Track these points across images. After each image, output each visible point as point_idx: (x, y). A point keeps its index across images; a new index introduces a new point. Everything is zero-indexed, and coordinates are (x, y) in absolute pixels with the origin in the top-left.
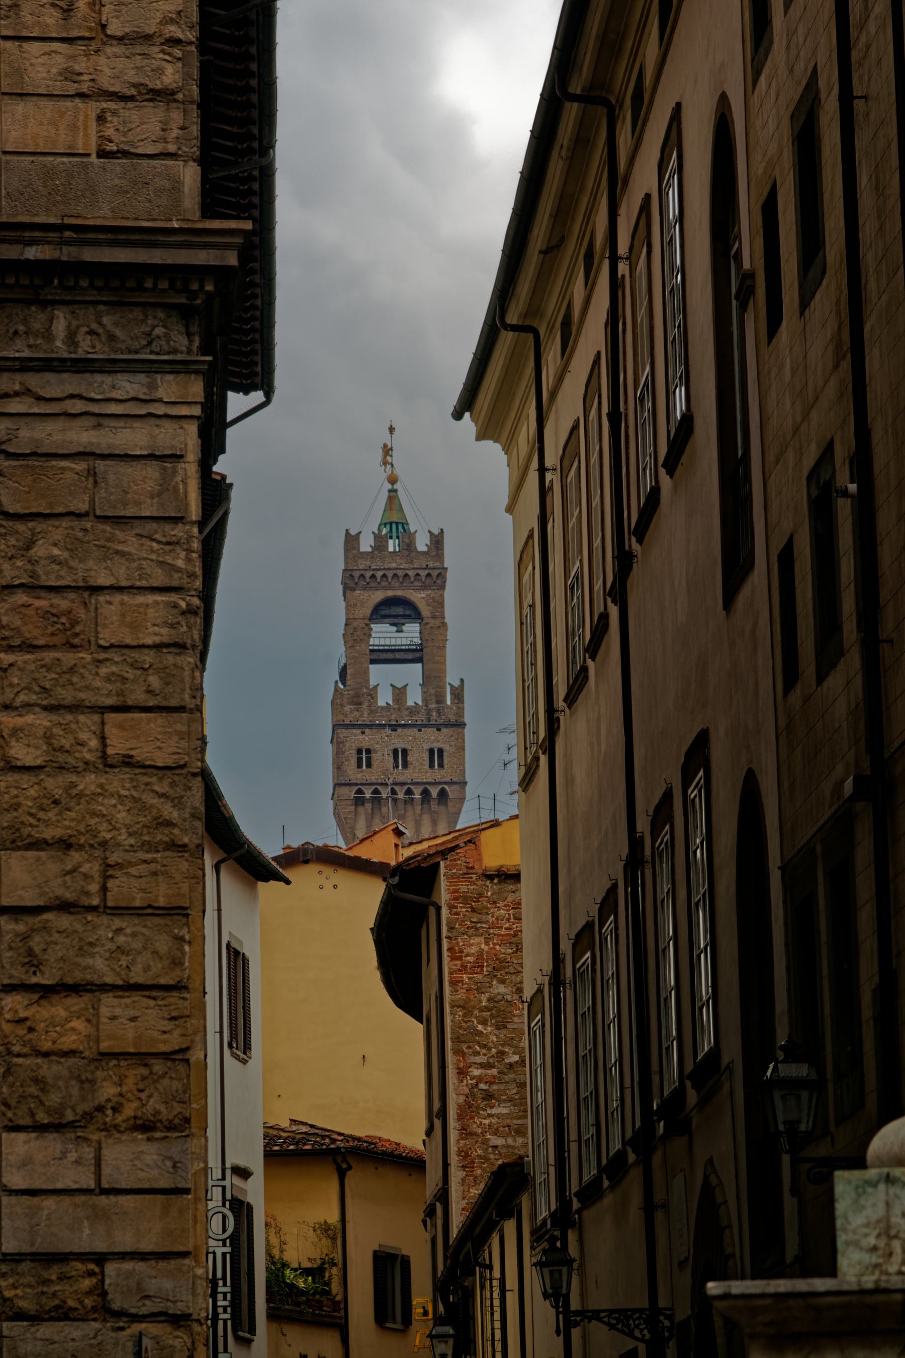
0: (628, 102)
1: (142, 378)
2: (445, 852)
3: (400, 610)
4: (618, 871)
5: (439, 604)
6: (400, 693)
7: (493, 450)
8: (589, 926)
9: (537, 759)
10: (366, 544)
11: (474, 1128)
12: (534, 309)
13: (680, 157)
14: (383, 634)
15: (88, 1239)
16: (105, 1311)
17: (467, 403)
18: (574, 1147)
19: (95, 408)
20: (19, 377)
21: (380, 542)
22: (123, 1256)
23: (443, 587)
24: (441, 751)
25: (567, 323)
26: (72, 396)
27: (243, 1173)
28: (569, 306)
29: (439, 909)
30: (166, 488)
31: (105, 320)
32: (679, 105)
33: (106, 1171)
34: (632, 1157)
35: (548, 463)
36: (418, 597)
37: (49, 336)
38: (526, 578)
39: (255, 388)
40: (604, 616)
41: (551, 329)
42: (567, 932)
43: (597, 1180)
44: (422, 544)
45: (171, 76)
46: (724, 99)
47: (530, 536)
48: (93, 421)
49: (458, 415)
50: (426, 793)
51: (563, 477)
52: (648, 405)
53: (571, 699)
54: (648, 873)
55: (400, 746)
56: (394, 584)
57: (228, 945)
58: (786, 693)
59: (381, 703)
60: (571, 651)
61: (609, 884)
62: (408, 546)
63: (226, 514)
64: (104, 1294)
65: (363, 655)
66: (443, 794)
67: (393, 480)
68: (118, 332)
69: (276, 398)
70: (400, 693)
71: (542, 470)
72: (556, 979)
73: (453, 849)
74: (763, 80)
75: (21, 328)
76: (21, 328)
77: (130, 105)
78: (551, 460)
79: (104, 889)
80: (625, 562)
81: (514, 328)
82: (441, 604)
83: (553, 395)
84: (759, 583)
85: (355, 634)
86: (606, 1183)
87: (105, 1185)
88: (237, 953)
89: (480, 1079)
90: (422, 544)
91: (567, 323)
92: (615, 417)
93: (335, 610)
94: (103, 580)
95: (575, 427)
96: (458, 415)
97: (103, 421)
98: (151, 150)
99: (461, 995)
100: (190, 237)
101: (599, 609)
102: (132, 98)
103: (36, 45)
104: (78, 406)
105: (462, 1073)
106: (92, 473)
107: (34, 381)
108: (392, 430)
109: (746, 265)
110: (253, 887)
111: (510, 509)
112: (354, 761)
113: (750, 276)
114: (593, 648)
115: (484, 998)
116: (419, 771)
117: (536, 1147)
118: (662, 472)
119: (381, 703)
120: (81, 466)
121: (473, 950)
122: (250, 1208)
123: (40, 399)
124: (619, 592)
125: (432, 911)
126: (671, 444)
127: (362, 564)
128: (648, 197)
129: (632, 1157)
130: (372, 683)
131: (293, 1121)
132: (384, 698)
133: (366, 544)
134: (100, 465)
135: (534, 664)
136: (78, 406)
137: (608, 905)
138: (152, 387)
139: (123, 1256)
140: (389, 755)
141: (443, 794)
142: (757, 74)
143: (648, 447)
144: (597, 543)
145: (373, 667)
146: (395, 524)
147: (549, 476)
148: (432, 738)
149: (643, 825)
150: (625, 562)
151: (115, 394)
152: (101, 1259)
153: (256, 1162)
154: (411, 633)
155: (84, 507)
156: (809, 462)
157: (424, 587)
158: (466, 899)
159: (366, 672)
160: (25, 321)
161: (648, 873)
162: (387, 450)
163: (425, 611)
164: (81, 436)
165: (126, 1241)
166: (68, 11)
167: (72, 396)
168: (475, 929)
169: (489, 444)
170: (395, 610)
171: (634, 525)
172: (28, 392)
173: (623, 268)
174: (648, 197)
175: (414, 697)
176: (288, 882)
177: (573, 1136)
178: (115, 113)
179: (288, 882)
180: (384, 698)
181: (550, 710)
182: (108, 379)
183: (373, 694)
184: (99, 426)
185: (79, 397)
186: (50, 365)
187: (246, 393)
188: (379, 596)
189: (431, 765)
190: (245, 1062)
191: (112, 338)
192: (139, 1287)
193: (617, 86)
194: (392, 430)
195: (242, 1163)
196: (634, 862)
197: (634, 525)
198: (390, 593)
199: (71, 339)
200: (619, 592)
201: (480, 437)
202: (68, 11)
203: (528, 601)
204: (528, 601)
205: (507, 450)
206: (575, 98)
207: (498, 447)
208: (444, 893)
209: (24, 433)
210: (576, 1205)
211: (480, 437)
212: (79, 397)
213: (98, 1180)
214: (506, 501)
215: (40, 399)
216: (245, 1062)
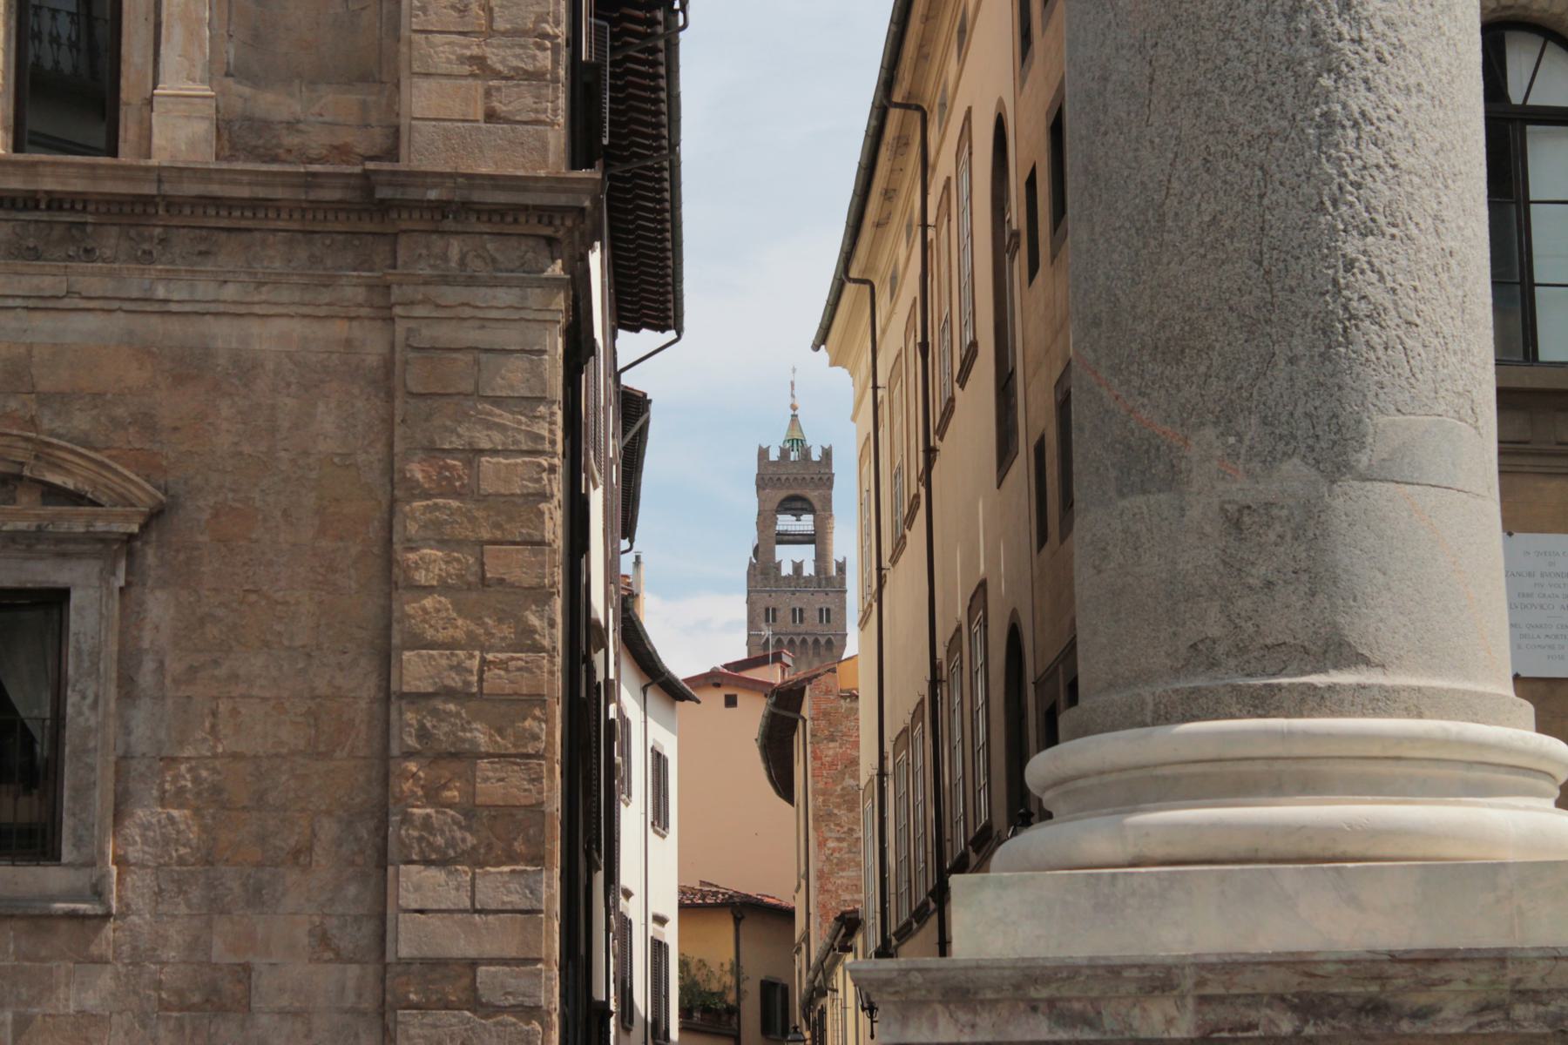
0: (936, 109)
1: (516, 291)
2: (809, 680)
3: (799, 505)
4: (925, 691)
5: (827, 501)
6: (798, 567)
7: (841, 373)
8: (905, 730)
9: (870, 605)
10: (774, 455)
11: (829, 886)
12: (870, 266)
13: (970, 147)
14: (786, 522)
15: (463, 947)
16: (475, 1003)
17: (822, 338)
18: (893, 897)
19: (480, 314)
20: (422, 289)
21: (784, 454)
22: (491, 961)
23: (831, 487)
24: (828, 610)
25: (894, 278)
26: (463, 304)
27: (661, 920)
28: (896, 266)
29: (805, 721)
30: (536, 373)
31: (489, 246)
32: (970, 109)
33: (479, 896)
34: (932, 906)
35: (879, 383)
36: (813, 495)
37: (445, 258)
38: (865, 470)
39: (669, 328)
40: (917, 496)
41: (883, 282)
42: (889, 736)
43: (909, 923)
44: (816, 455)
45: (545, 60)
46: (1001, 102)
47: (868, 438)
48: (478, 323)
49: (816, 347)
50: (816, 641)
51: (891, 392)
52: (947, 337)
53: (894, 560)
54: (945, 689)
55: (798, 605)
56: (792, 485)
57: (653, 749)
58: (1039, 551)
59: (784, 573)
60: (895, 525)
61: (918, 699)
62: (806, 454)
63: (647, 422)
64: (475, 990)
65: (769, 538)
66: (829, 642)
67: (794, 408)
68: (498, 256)
69: (685, 335)
70: (798, 567)
71: (875, 388)
72: (882, 774)
73: (816, 676)
74: (1027, 87)
75: (424, 252)
76: (424, 252)
77: (510, 83)
78: (882, 380)
79: (481, 680)
80: (930, 453)
81: (855, 281)
82: (830, 501)
83: (884, 332)
84: (1022, 466)
85: (765, 521)
86: (915, 925)
87: (478, 906)
88: (659, 755)
89: (834, 850)
90: (816, 455)
91: (894, 278)
92: (924, 347)
93: (748, 503)
94: (485, 444)
95: (899, 355)
96: (816, 347)
97: (486, 323)
98: (523, 117)
99: (821, 785)
100: (554, 183)
101: (913, 491)
102: (512, 78)
103: (439, 36)
104: (468, 312)
105: (822, 844)
106: (477, 362)
107: (432, 291)
108: (794, 370)
109: (1014, 227)
110: (673, 705)
111: (854, 419)
112: (763, 616)
113: (1016, 235)
114: (909, 520)
115: (839, 788)
116: (811, 623)
117: (868, 904)
118: (956, 386)
119: (784, 573)
120: (469, 358)
121: (831, 753)
122: (666, 946)
123: (438, 306)
124: (926, 478)
125: (800, 723)
126: (963, 363)
127: (771, 470)
128: (949, 179)
129: (932, 906)
130: (778, 559)
131: (702, 883)
132: (787, 570)
133: (774, 455)
134: (483, 357)
135: (869, 535)
136: (468, 312)
137: (917, 714)
138: (524, 298)
139: (491, 961)
140: (790, 616)
141: (829, 642)
142: (1023, 80)
143: (946, 363)
144: (913, 442)
145: (778, 548)
146: (797, 442)
147: (880, 393)
148: (821, 601)
149: (941, 653)
150: (930, 453)
151: (495, 303)
152: (473, 964)
153: (672, 913)
154: (806, 523)
155: (470, 388)
156: (1056, 374)
157: (817, 487)
158: (826, 714)
159: (773, 551)
160: (428, 247)
161: (945, 689)
162: (793, 384)
163: (818, 506)
164: (471, 335)
165: (491, 949)
166: (463, 11)
167: (463, 304)
168: (832, 738)
169: (839, 370)
170: (795, 505)
171: (934, 428)
172: (424, 302)
173: (931, 233)
174: (949, 179)
175: (809, 570)
176: (698, 702)
177: (893, 890)
178: (498, 89)
179: (698, 702)
180: (787, 570)
181: (880, 568)
182: (489, 291)
183: (778, 567)
184: (483, 327)
185: (467, 304)
186: (445, 280)
187: (663, 331)
188: (783, 494)
189: (821, 620)
190: (663, 837)
191: (494, 260)
192: (502, 986)
193: (928, 95)
194: (794, 370)
195: (661, 912)
196: (935, 682)
197: (934, 428)
198: (792, 492)
199: (462, 262)
200: (926, 478)
201: (833, 363)
202: (463, 11)
203: (866, 487)
204: (866, 487)
205: (852, 374)
206: (897, 105)
207: (845, 372)
208: (807, 710)
209: (425, 332)
210: (894, 942)
211: (833, 363)
212: (467, 304)
213: (473, 904)
214: (851, 412)
215: (438, 306)
216: (663, 837)
